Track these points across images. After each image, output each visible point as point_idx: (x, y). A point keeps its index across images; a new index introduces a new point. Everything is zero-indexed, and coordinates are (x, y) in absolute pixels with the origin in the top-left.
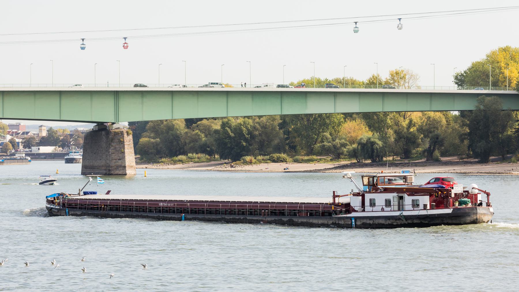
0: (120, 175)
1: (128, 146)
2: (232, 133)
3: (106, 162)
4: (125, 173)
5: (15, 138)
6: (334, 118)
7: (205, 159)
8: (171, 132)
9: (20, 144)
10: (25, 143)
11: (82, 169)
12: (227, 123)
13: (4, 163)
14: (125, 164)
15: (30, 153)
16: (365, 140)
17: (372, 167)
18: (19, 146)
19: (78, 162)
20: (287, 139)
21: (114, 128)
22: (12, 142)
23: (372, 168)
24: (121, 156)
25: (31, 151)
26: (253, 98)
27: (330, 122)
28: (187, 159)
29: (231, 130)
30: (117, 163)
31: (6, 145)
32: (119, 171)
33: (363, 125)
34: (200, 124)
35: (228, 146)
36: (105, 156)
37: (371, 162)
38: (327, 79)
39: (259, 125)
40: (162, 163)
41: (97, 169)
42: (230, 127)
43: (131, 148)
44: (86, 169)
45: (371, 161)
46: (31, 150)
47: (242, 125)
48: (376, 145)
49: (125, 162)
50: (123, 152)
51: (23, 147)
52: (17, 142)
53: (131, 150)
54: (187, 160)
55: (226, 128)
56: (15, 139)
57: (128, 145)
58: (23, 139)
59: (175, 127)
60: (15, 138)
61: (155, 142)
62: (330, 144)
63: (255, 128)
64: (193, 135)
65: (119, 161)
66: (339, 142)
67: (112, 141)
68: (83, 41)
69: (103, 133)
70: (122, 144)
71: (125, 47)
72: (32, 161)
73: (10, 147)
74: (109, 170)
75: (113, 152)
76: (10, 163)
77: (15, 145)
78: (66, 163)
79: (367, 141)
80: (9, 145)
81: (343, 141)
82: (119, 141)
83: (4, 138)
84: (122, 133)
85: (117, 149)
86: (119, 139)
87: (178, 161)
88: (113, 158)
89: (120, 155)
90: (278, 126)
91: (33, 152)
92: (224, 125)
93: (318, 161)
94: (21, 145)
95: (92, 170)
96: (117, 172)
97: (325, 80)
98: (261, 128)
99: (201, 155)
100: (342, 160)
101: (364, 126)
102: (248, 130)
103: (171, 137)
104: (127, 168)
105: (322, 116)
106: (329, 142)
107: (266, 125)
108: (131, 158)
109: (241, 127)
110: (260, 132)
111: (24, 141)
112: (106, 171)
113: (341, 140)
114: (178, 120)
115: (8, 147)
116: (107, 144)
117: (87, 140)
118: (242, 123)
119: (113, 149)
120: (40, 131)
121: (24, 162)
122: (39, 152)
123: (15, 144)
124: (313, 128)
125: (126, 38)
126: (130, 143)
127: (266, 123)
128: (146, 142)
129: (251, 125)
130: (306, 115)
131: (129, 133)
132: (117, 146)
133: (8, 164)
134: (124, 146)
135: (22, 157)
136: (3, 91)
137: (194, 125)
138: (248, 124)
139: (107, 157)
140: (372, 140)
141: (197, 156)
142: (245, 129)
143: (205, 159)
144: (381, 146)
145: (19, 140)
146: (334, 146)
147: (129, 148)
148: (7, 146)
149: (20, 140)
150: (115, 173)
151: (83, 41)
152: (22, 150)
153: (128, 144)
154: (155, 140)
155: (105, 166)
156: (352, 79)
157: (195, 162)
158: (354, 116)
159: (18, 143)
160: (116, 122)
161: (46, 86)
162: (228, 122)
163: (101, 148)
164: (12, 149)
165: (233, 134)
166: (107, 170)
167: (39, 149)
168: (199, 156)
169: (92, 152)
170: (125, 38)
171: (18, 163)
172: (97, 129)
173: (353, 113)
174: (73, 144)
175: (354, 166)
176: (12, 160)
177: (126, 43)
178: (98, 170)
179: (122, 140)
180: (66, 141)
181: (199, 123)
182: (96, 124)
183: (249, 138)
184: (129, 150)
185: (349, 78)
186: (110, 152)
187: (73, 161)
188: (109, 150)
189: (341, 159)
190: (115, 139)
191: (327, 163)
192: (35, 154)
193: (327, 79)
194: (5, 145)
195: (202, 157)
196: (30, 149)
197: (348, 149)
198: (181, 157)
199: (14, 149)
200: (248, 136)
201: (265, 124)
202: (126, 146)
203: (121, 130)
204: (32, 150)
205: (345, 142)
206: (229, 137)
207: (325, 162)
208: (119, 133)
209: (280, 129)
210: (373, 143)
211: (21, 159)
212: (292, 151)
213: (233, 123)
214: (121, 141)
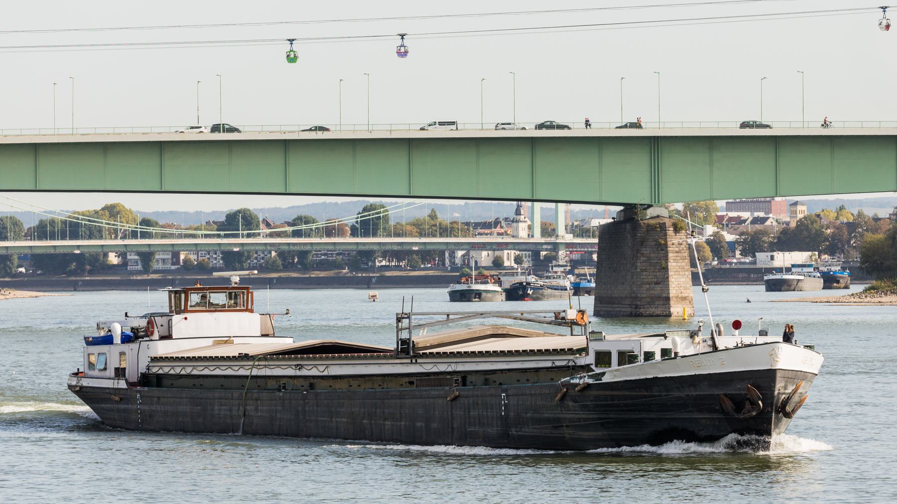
0: (658, 316)
1: (675, 254)
3: (631, 290)
4: (667, 312)
11: (595, 304)
14: (669, 294)
15: (735, 267)
19: (793, 287)
21: (648, 217)
24: (659, 277)
25: (755, 263)
30: (652, 292)
32: (656, 308)
40: (872, 291)
41: (619, 304)
43: (683, 258)
44: (601, 304)
49: (669, 290)
50: (664, 268)
52: (727, 240)
53: (684, 264)
56: (722, 235)
57: (677, 252)
58: (741, 234)
65: (657, 286)
67: (642, 244)
68: (402, 38)
69: (628, 226)
70: (663, 250)
71: (292, 58)
73: (706, 255)
74: (637, 307)
75: (644, 268)
77: (722, 249)
78: (767, 290)
80: (704, 248)
82: (656, 245)
84: (663, 227)
85: (652, 261)
86: (656, 241)
89: (658, 274)
91: (759, 266)
95: (610, 305)
96: (652, 310)
104: (672, 303)
108: (683, 280)
111: (742, 240)
112: (632, 307)
119: (644, 262)
120: (793, 215)
122: (772, 264)
123: (722, 247)
126: (681, 249)
128: (93, 253)
131: (679, 226)
132: (652, 255)
134: (668, 255)
136: (409, 139)
150: (647, 313)
151: (402, 38)
153: (677, 249)
155: (630, 298)
163: (625, 258)
164: (711, 258)
166: (633, 306)
167: (772, 258)
170: (291, 41)
172: (622, 219)
174: (854, 245)
178: (619, 306)
179: (663, 242)
180: (838, 240)
182: (622, 208)
184: (679, 264)
186: (638, 268)
187: (782, 286)
188: (637, 262)
190: (648, 239)
192: (762, 268)
199: (716, 259)
202: (670, 255)
203: (662, 220)
208: (656, 227)
214: (660, 244)
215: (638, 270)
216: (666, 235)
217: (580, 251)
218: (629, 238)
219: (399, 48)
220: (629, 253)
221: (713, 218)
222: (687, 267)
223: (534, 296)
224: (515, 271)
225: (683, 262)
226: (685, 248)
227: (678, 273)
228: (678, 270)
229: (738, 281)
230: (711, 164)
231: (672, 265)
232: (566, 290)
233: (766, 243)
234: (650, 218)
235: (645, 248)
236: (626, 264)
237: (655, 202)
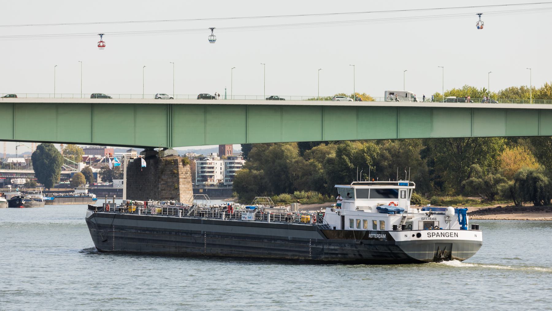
1: (183, 180)
2: (351, 163)
5: (91, 167)
6: (493, 143)
7: (317, 199)
8: (277, 161)
9: (98, 175)
10: (106, 174)
12: (345, 149)
13: (54, 202)
16: (525, 175)
17: (523, 212)
18: (96, 178)
20: (431, 172)
21: (165, 156)
22: (86, 172)
23: (523, 213)
24: (173, 194)
25: (112, 185)
26: (357, 115)
27: (488, 149)
28: (292, 199)
29: (350, 159)
31: (78, 176)
33: (528, 154)
34: (316, 150)
35: (345, 181)
36: (153, 194)
37: (533, 206)
38: (486, 88)
39: (389, 152)
42: (348, 155)
43: (188, 183)
45: (533, 205)
46: (113, 184)
47: (365, 153)
48: (540, 183)
50: (176, 189)
51: (102, 180)
53: (189, 186)
54: (292, 201)
55: (343, 157)
56: (91, 169)
57: (184, 178)
58: (102, 168)
59: (285, 154)
60: (91, 167)
61: (259, 175)
62: (481, 180)
63: (384, 156)
64: (307, 165)
66: (493, 177)
67: (162, 173)
70: (176, 177)
71: (101, 45)
72: (98, 200)
75: (163, 188)
76: (64, 203)
79: (528, 176)
80: (81, 176)
81: (499, 175)
82: (171, 174)
83: (76, 166)
85: (169, 184)
86: (172, 171)
87: (279, 202)
88: (164, 196)
89: (172, 192)
90: (420, 154)
91: (114, 187)
92: (340, 152)
93: (463, 203)
94: (99, 177)
97: (482, 91)
98: (392, 157)
99: (312, 193)
100: (496, 202)
101: (529, 156)
102: (373, 159)
103: (278, 168)
105: (477, 141)
106: (480, 177)
107: (399, 152)
109: (364, 155)
110: (390, 163)
111: (103, 172)
113: (495, 175)
114: (290, 145)
115: (80, 179)
116: (156, 177)
117: (132, 171)
118: (365, 149)
119: (163, 184)
121: (85, 201)
123: (90, 176)
124: (465, 157)
125: (102, 35)
126: (187, 176)
127: (399, 149)
129: (378, 152)
130: (455, 139)
131: (186, 162)
132: (168, 180)
133: (60, 203)
134: (179, 181)
135: (84, 193)
137: (307, 151)
138: (374, 151)
139: (155, 195)
140: (535, 175)
141: (306, 194)
142: (369, 157)
143: (317, 199)
144: (547, 182)
145: (96, 169)
146: (486, 183)
147: (186, 182)
148: (78, 178)
149: (99, 170)
152: (99, 184)
153: (184, 177)
154: (258, 172)
156: (533, 88)
157: (303, 204)
158: (520, 140)
159: (96, 174)
160: (168, 147)
161: (72, 97)
162: (346, 148)
164: (85, 182)
165: (352, 165)
168: (309, 195)
169: (137, 188)
171: (76, 202)
173: (519, 137)
175: (499, 211)
176: (66, 199)
177: (212, 35)
179: (176, 172)
181: (314, 148)
182: (143, 150)
183: (375, 171)
184: (186, 186)
185: (529, 87)
186: (160, 188)
188: (159, 185)
189: (495, 200)
190: (166, 170)
191: (474, 207)
193: (486, 88)
194: (75, 176)
195: (313, 197)
196: (111, 183)
197: (502, 186)
198: (283, 196)
199: (88, 183)
200: (373, 167)
201: (398, 150)
202: (181, 180)
203: (175, 158)
204: (114, 185)
205: (502, 178)
206: (348, 168)
207: (472, 205)
208: (171, 162)
209: (422, 158)
210: (536, 180)
211: (80, 197)
212: (437, 189)
213: (353, 149)
214: (174, 173)
215: (160, 190)
216: (178, 167)
217: (4, 177)
218: (152, 169)
219: (99, 43)
220: (153, 178)
221: (81, 158)
222: (191, 188)
223: (26, 205)
224: (9, 189)
225: (188, 185)
226: (189, 176)
227: (185, 192)
228: (185, 190)
229: (102, 197)
230: (205, 122)
231: (181, 186)
232: (41, 201)
233: (117, 174)
234: (167, 156)
235: (164, 175)
236: (150, 185)
237: (170, 146)
